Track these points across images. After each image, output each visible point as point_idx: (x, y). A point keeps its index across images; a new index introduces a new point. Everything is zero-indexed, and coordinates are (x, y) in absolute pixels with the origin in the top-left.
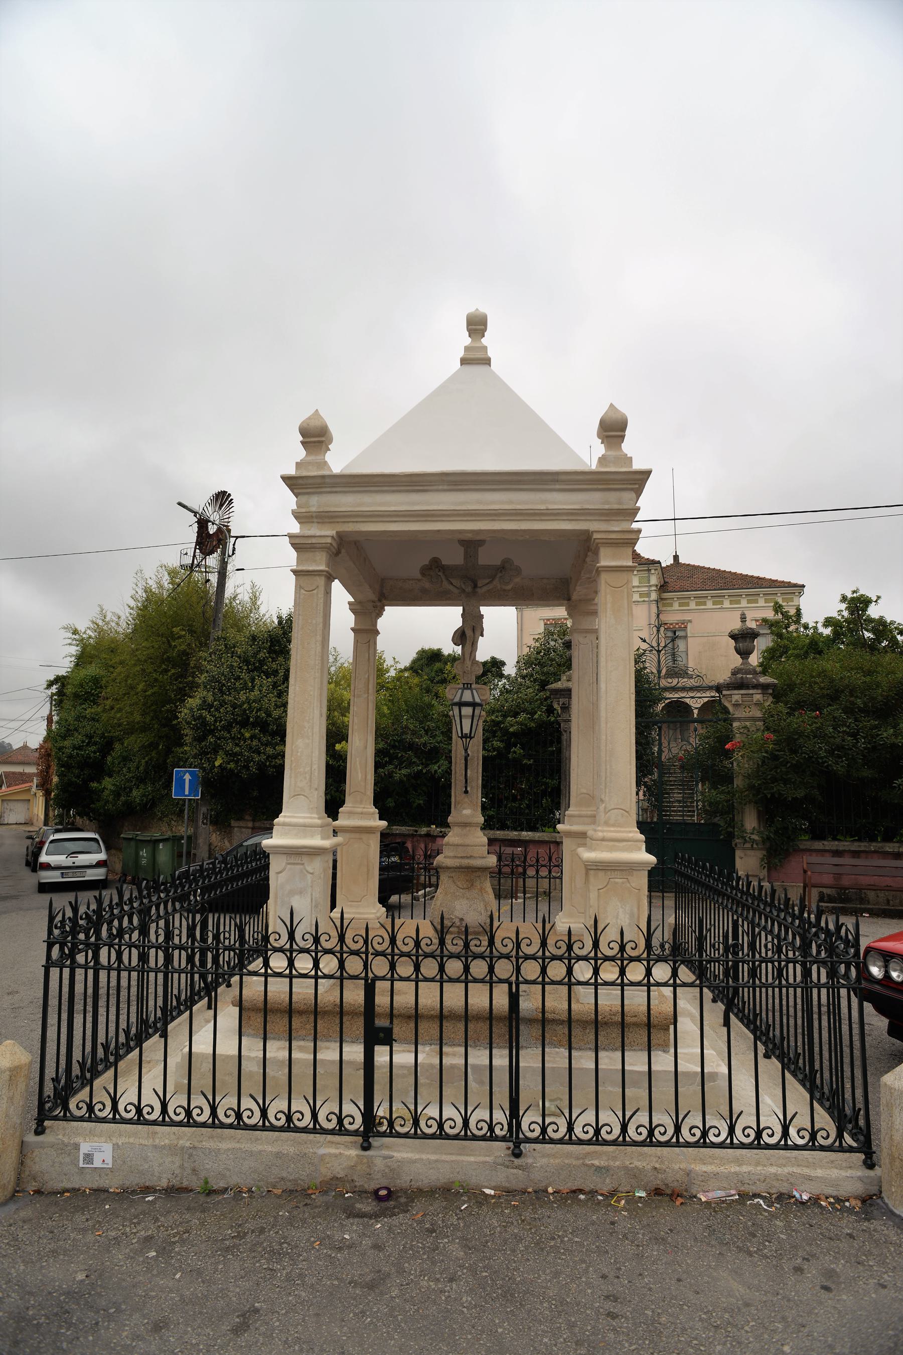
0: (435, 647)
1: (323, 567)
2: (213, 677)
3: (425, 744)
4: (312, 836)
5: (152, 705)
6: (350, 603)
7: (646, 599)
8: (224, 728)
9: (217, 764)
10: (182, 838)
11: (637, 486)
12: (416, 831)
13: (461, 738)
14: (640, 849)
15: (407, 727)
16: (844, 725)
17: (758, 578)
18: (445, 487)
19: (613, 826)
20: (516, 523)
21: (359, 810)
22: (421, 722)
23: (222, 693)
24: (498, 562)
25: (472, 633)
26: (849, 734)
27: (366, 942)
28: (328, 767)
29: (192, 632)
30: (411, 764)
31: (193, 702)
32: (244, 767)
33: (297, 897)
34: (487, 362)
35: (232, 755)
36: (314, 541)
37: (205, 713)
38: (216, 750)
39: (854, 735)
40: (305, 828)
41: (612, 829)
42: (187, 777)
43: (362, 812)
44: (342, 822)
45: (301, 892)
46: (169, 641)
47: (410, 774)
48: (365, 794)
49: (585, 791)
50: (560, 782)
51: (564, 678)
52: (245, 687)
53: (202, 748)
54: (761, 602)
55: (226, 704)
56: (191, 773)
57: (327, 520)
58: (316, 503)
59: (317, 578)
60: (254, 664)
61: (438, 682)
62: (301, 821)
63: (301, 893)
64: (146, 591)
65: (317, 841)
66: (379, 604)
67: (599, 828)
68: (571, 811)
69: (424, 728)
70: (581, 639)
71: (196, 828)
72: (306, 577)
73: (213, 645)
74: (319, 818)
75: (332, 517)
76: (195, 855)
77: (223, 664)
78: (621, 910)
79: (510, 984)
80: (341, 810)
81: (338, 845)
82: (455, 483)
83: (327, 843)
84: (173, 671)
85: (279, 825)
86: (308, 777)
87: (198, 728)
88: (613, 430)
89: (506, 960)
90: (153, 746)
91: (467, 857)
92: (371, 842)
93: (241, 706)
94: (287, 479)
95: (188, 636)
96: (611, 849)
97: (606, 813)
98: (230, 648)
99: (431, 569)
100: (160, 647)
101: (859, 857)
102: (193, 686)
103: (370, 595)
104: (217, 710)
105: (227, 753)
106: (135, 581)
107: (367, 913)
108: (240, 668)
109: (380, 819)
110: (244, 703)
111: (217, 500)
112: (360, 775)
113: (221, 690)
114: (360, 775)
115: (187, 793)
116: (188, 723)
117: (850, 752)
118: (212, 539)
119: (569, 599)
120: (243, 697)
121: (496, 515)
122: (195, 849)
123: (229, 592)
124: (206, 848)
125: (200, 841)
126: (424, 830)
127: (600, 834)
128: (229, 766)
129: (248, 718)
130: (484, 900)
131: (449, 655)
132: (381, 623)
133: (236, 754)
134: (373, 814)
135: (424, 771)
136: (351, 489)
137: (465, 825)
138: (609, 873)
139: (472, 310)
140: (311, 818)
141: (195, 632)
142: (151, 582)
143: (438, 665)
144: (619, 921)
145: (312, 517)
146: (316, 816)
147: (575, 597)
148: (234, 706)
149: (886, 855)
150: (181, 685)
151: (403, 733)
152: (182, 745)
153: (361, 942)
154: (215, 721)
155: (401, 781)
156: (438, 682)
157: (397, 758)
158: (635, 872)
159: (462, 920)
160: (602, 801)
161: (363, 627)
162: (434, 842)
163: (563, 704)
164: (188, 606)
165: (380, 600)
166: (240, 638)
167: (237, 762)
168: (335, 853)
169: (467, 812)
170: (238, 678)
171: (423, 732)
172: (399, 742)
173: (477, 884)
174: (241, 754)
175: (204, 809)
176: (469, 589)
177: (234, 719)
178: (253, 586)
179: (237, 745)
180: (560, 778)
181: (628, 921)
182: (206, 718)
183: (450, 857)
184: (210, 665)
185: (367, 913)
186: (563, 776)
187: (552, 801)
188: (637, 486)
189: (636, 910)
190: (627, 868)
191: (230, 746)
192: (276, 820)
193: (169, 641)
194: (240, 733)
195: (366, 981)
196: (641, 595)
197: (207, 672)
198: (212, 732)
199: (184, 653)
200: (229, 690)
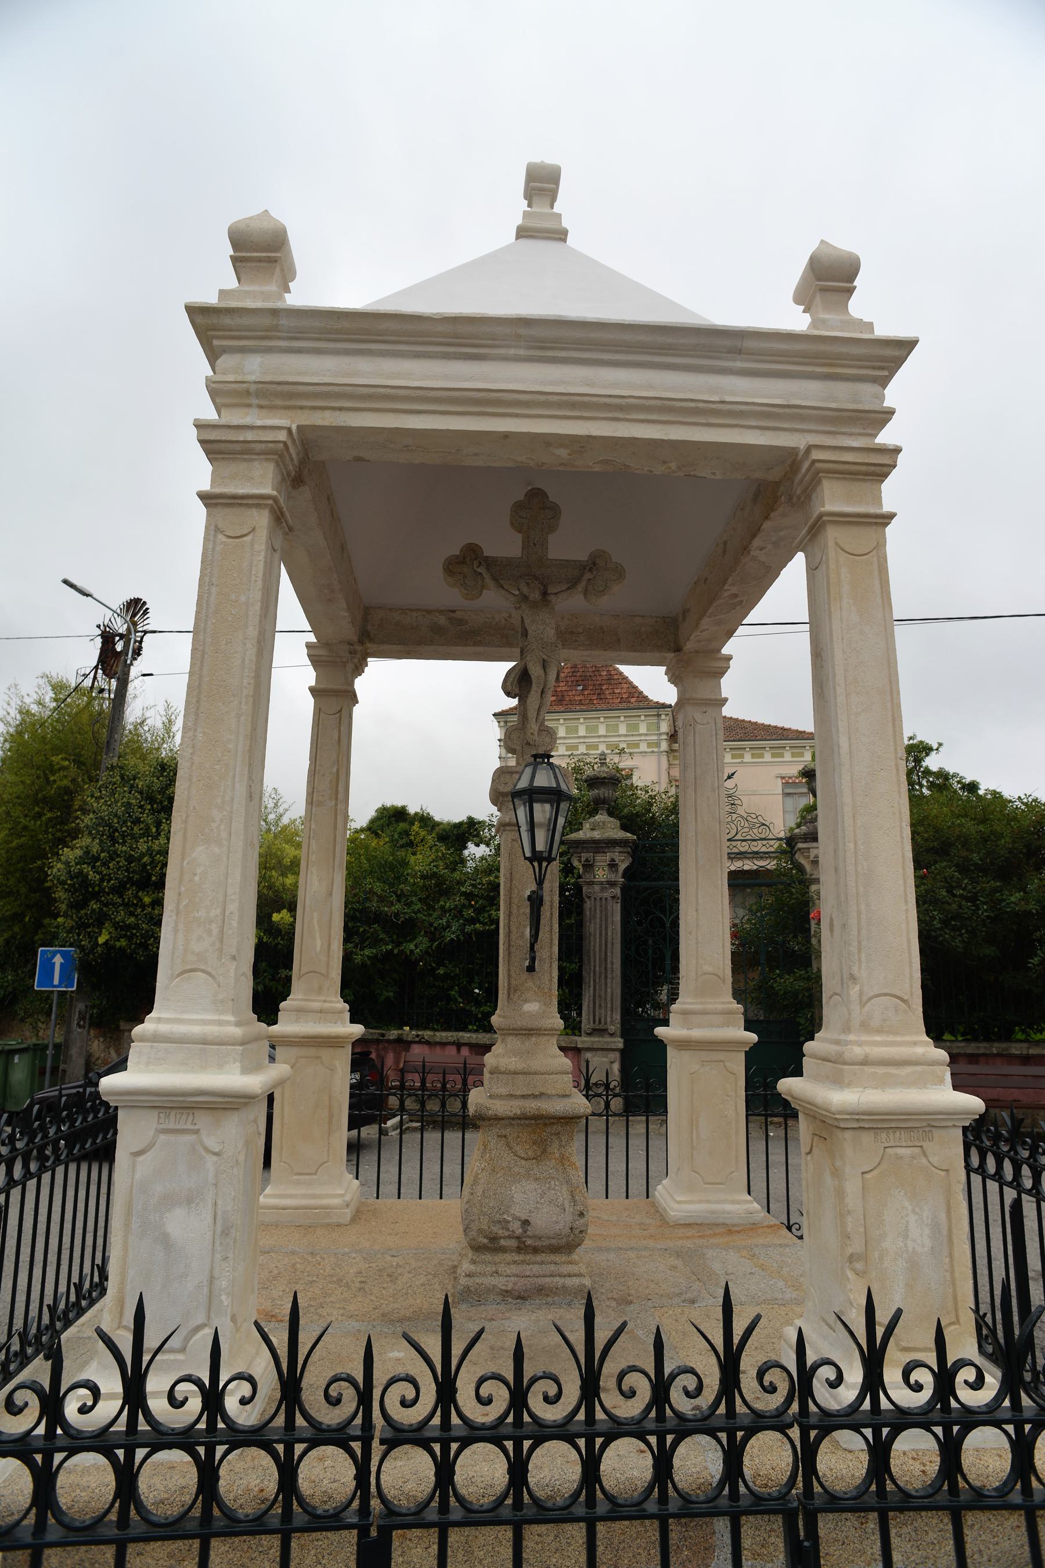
0: (399, 803)
1: (268, 490)
2: (102, 818)
3: (397, 915)
4: (220, 1066)
5: (19, 862)
6: (309, 646)
7: (656, 750)
8: (114, 890)
9: (101, 940)
10: (46, 1047)
11: (886, 373)
12: (383, 1035)
13: (530, 860)
14: (941, 1081)
15: (371, 891)
16: (960, 887)
17: (782, 729)
18: (522, 352)
19: (879, 1031)
20: (659, 427)
21: (317, 1005)
22: (391, 885)
23: (114, 841)
24: (583, 556)
25: (541, 672)
26: (967, 899)
27: (365, 1398)
28: (261, 950)
29: (79, 763)
30: (377, 942)
31: (70, 854)
32: (141, 944)
33: (179, 1212)
34: (561, 235)
35: (122, 928)
36: (250, 436)
37: (86, 869)
38: (100, 920)
39: (973, 899)
40: (203, 1048)
41: (878, 1038)
42: (58, 960)
43: (319, 1009)
44: (285, 1026)
45: (190, 1200)
46: (45, 775)
47: (376, 956)
48: (326, 976)
49: (710, 969)
50: (581, 967)
51: (587, 826)
52: (147, 833)
53: (81, 918)
54: (788, 756)
55: (118, 856)
56: (64, 955)
57: (279, 402)
58: (255, 367)
59: (254, 512)
60: (161, 802)
61: (402, 846)
62: (196, 1030)
63: (189, 1201)
64: (20, 712)
65: (232, 1078)
66: (359, 648)
67: (852, 1037)
68: (153, 1015)
69: (395, 893)
70: (698, 716)
71: (69, 1032)
72: (228, 510)
73: (104, 777)
74: (238, 1024)
75: (291, 396)
76: (64, 1071)
77: (116, 802)
78: (912, 1219)
79: (790, 1518)
80: (282, 1005)
81: (281, 1083)
82: (541, 344)
83: (255, 1082)
84: (49, 815)
85: (143, 1039)
86: (215, 929)
87: (76, 890)
88: (830, 278)
89: (778, 1435)
90: (17, 917)
91: (535, 1097)
92: (337, 1063)
93: (140, 859)
94: (195, 312)
95: (73, 770)
96: (884, 1083)
97: (863, 1005)
98: (128, 780)
99: (464, 562)
100: (33, 783)
101: (977, 1063)
102: (75, 834)
103: (350, 632)
104: (104, 864)
105: (116, 925)
106: (7, 699)
107: (327, 1196)
108: (141, 807)
109: (352, 1022)
110: (143, 855)
111: (127, 611)
112: (319, 943)
113: (112, 838)
114: (319, 943)
115: (56, 982)
116: (63, 883)
117: (969, 922)
118: (116, 655)
119: (678, 649)
120: (142, 847)
121: (620, 408)
122: (65, 1063)
123: (132, 713)
124: (81, 1061)
125: (74, 1051)
126: (393, 1034)
127: (858, 1051)
128: (118, 944)
129: (150, 876)
130: (568, 1182)
131: (416, 814)
132: (360, 684)
133: (129, 927)
134: (341, 1012)
135: (396, 951)
136: (331, 345)
137: (528, 1032)
138: (884, 1135)
139: (537, 159)
140: (220, 1023)
141: (84, 764)
142: (27, 700)
143: (402, 825)
144: (910, 1243)
145: (248, 393)
146: (231, 1018)
147: (689, 646)
148: (130, 859)
149: (1010, 1059)
150: (59, 834)
151: (367, 899)
152: (56, 916)
153: (350, 1396)
154: (102, 880)
155: (364, 965)
156: (402, 846)
157: (357, 933)
158: (936, 1133)
159: (526, 1223)
160: (852, 977)
161: (330, 686)
162: (407, 1050)
163: (587, 860)
164: (75, 729)
165: (361, 642)
166: (143, 768)
167: (130, 939)
168: (271, 1098)
169: (532, 1007)
170: (137, 821)
171: (394, 898)
172: (361, 911)
173: (554, 1149)
174: (136, 926)
175: (81, 1006)
176: (536, 596)
177: (129, 878)
178: (168, 706)
179: (132, 914)
180: (581, 961)
181: (928, 1243)
182: (87, 875)
183: (500, 1097)
184: (98, 805)
185: (327, 1196)
186: (585, 958)
187: (571, 992)
188: (886, 373)
189: (943, 1216)
190: (917, 1124)
191: (121, 915)
192: (138, 1030)
193: (45, 775)
194: (136, 896)
195: (363, 1531)
196: (649, 745)
197: (94, 812)
198: (96, 896)
199: (67, 791)
200: (123, 837)
